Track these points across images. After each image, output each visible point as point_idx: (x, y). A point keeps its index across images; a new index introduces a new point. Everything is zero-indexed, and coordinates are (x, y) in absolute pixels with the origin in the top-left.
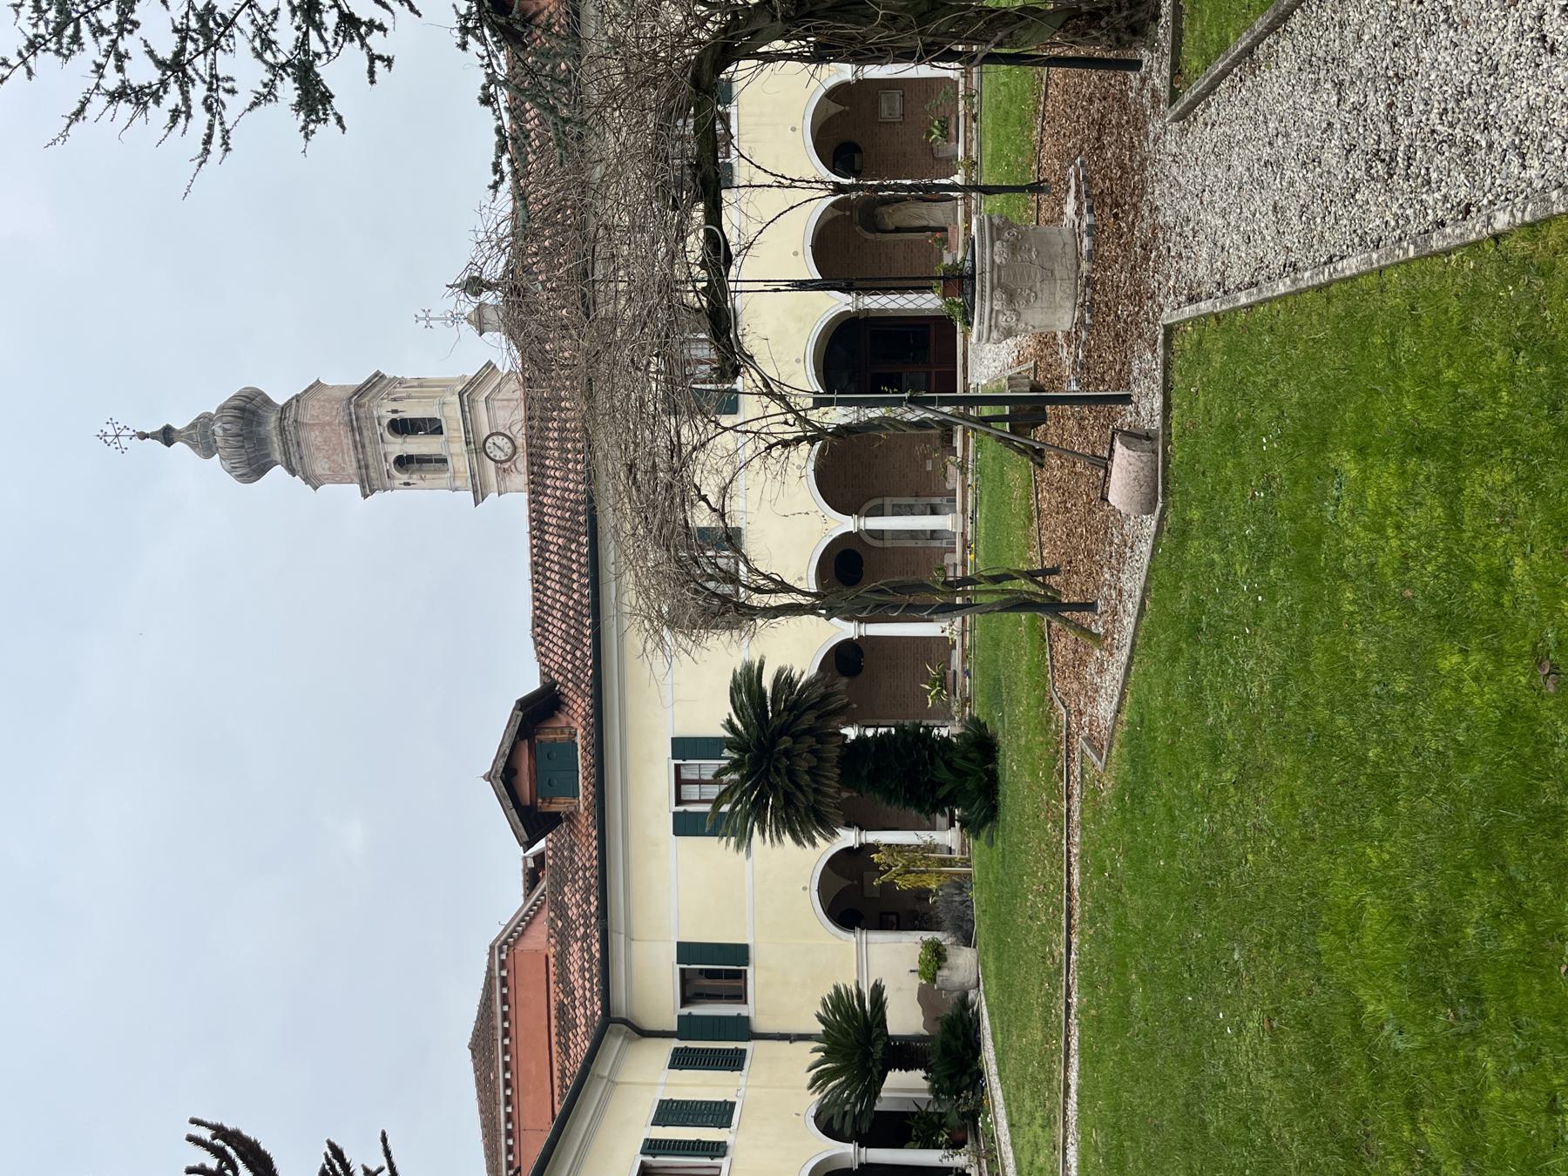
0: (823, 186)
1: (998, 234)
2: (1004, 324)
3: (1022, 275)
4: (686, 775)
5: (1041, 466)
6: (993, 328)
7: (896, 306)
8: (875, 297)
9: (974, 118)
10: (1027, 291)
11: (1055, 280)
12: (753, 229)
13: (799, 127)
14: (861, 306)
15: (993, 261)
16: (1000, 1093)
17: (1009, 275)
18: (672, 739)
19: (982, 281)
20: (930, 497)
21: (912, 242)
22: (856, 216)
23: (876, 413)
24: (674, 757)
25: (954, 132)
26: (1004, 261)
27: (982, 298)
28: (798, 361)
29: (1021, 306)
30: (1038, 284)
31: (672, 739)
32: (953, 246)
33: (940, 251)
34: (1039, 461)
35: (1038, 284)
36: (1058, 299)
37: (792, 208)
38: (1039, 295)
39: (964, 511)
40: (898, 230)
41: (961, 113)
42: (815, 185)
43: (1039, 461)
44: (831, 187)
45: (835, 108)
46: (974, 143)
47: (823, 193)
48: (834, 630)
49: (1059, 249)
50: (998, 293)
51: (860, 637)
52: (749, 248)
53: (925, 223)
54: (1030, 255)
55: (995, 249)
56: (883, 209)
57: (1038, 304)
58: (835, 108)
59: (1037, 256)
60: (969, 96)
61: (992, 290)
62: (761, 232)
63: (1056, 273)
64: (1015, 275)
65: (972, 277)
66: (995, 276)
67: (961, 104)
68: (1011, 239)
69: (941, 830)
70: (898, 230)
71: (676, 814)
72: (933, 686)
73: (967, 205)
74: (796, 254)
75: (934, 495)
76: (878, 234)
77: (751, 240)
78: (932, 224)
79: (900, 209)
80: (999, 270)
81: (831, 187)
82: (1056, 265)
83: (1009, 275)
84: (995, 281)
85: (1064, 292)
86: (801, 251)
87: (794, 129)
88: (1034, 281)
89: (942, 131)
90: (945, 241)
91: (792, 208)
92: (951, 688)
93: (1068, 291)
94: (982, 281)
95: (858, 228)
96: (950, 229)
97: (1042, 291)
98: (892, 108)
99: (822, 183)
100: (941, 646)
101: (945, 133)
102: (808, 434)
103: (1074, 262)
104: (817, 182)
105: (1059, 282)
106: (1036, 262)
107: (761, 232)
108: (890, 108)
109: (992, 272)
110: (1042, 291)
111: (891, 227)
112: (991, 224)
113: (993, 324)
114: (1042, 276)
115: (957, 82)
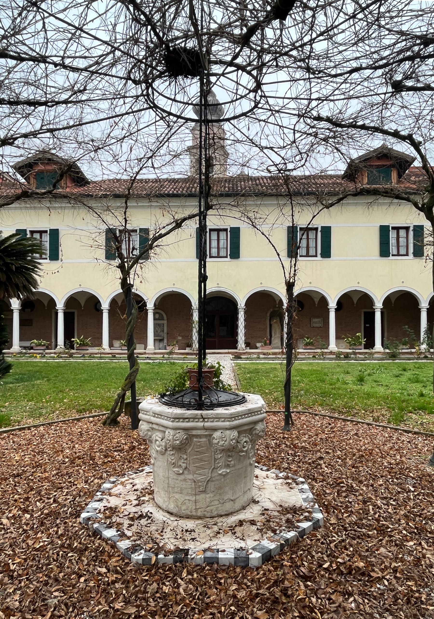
0: (292, 275)
1: (245, 431)
2: (154, 437)
3: (201, 460)
4: (44, 235)
5: (104, 424)
6: (151, 425)
7: (239, 325)
8: (243, 316)
9: (314, 357)
10: (184, 465)
11: (196, 495)
12: (265, 228)
13: (311, 285)
14: (240, 310)
15: (215, 429)
16: (194, 338)
17: (201, 446)
18: (58, 229)
19: (194, 418)
20: (158, 340)
21: (266, 331)
22: (276, 309)
23: (196, 317)
24: (50, 230)
25: (308, 348)
26: (215, 441)
27: (177, 418)
28: (218, 284)
29: (171, 457)
30: (191, 477)
31: (58, 229)
32: (263, 348)
33: (262, 342)
34: (108, 422)
35: (191, 477)
36: (177, 496)
37: (278, 255)
38: (182, 477)
39: (155, 354)
40: (271, 325)
41: (316, 351)
42: (293, 269)
43: (107, 423)
44: (291, 281)
45: (317, 301)
46: (304, 356)
47: (287, 276)
48: (105, 299)
49: (230, 496)
50: (181, 435)
51: (102, 310)
52: (253, 225)
53: (273, 335)
54: (221, 467)
55: (228, 432)
56: (278, 319)
57: (172, 475)
58: (317, 301)
59: (220, 475)
60: (323, 354)
61: (185, 429)
62: (263, 234)
63: (203, 496)
64: (201, 453)
65: (200, 406)
66: (199, 432)
67: (319, 351)
68: (240, 446)
69: (20, 344)
70: (271, 325)
71: (25, 230)
72: (81, 341)
73: (279, 353)
74: (261, 283)
75: (168, 340)
76: (269, 318)
77: (258, 227)
78: (273, 339)
79: (278, 326)
80: (206, 436)
81: (291, 281)
82: (212, 495)
83: (201, 446)
84: (194, 432)
85: (183, 503)
86: (262, 285)
87: (310, 283)
88: (194, 473)
89: (308, 343)
90: (265, 344)
91: (278, 255)
92: (80, 348)
93: (184, 508)
94: (194, 418)
95: (272, 310)
96: (270, 347)
97: (185, 480)
98: (316, 323)
99: (295, 275)
100: (99, 344)
101: (307, 344)
102: (126, 264)
103: (215, 513)
104: (295, 271)
105: (194, 498)
106: (215, 474)
107: (263, 234)
108: (317, 322)
109: (204, 428)
110: (185, 480)
111: (272, 323)
112: (256, 423)
113: (154, 426)
114: (199, 481)
115: (327, 348)
